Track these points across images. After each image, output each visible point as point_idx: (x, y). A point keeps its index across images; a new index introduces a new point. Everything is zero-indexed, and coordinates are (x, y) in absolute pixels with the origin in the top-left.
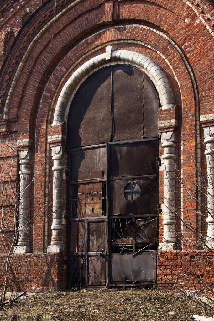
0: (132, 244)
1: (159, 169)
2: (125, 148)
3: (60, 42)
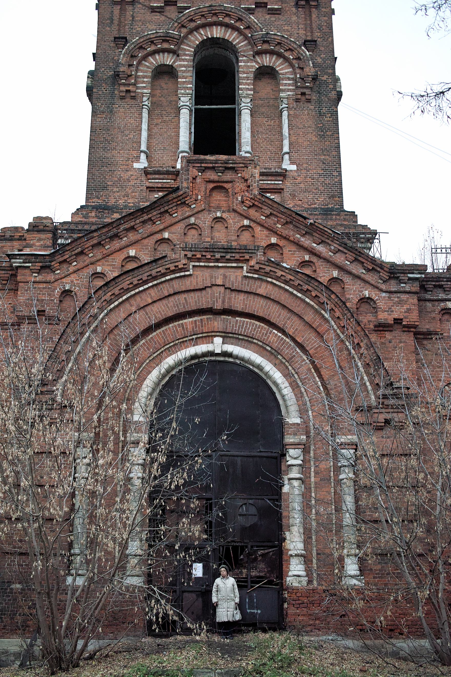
0: (247, 578)
1: (281, 490)
2: (239, 459)
3: (146, 319)
